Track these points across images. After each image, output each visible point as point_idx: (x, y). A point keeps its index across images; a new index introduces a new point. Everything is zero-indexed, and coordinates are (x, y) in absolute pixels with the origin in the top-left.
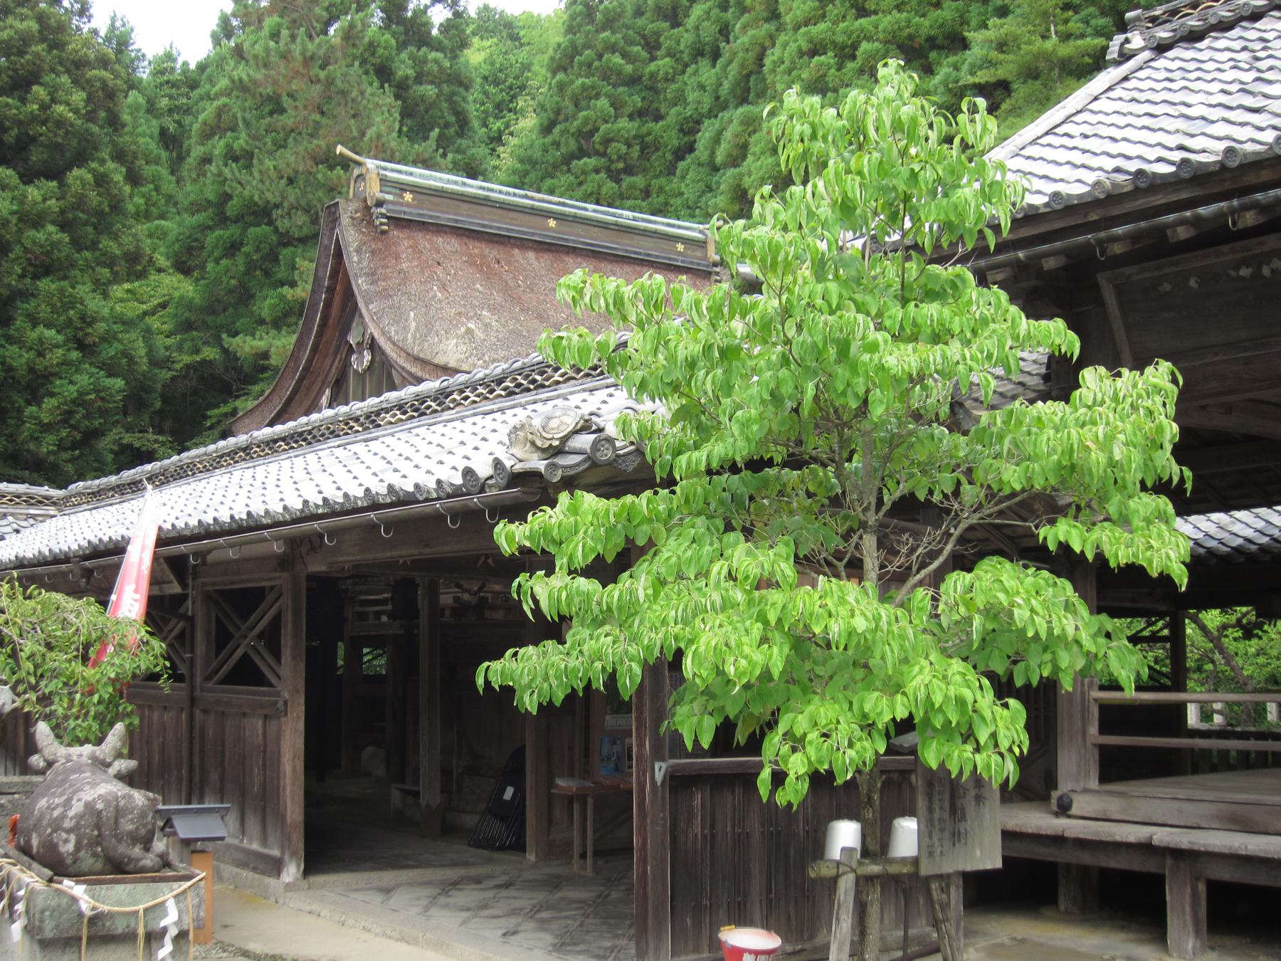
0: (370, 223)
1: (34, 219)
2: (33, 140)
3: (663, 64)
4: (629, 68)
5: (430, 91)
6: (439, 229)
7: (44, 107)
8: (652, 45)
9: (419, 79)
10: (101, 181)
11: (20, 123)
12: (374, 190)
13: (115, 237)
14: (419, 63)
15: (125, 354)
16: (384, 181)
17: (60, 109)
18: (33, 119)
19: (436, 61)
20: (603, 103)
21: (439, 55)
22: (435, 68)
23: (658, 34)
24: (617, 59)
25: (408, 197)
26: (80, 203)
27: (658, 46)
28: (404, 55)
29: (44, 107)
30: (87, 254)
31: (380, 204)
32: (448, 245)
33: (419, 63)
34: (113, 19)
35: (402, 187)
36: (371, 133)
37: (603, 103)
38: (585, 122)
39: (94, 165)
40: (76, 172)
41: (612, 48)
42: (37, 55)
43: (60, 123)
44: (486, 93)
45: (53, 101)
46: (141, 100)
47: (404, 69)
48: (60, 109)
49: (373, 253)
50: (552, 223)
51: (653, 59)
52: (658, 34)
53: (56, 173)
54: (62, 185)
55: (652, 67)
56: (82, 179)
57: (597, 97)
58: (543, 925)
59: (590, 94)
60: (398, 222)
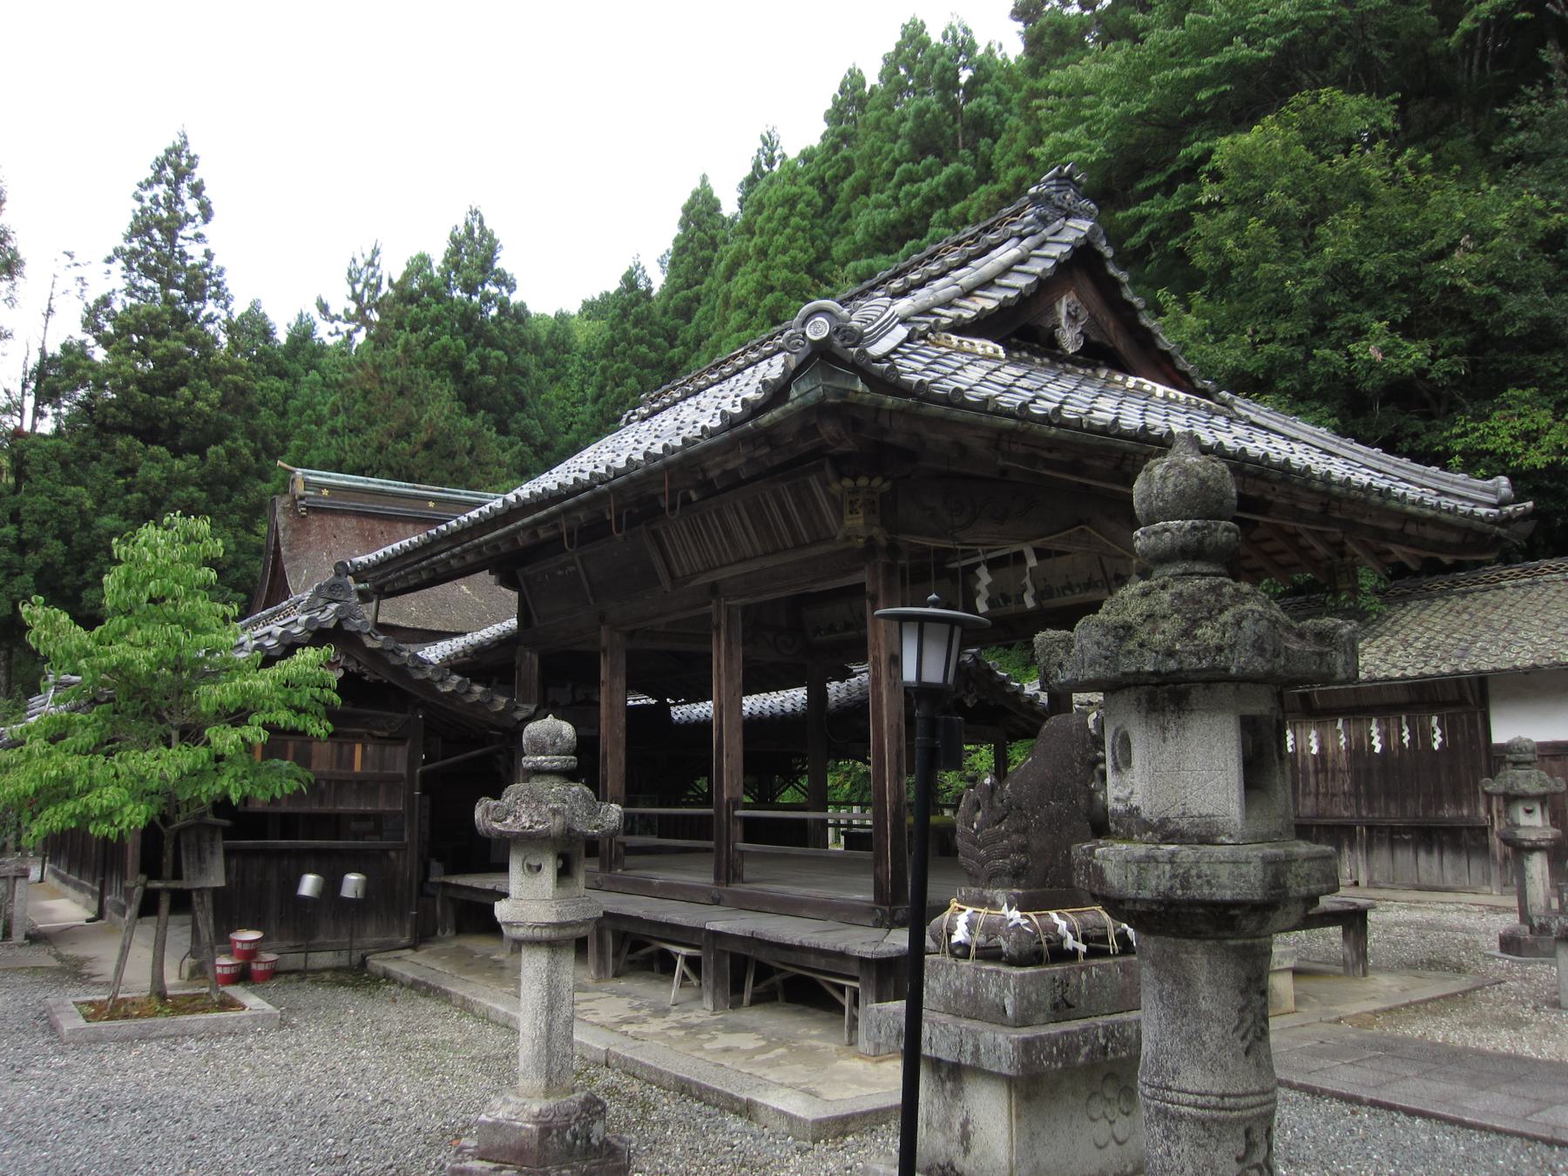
0: (296, 511)
1: (185, 481)
2: (182, 426)
3: (676, 352)
4: (653, 355)
5: (490, 380)
6: (345, 513)
7: (189, 403)
8: (671, 339)
9: (483, 371)
10: (232, 454)
11: (170, 415)
12: (300, 489)
13: (245, 493)
14: (483, 360)
15: (250, 575)
16: (307, 483)
17: (199, 404)
18: (181, 412)
19: (497, 358)
20: (632, 381)
21: (500, 353)
22: (495, 363)
23: (676, 329)
24: (644, 349)
25: (325, 492)
26: (215, 470)
27: (676, 339)
28: (473, 355)
29: (189, 403)
30: (223, 506)
31: (302, 498)
32: (349, 523)
33: (483, 360)
34: (301, 316)
35: (321, 486)
36: (426, 417)
37: (632, 381)
38: (619, 396)
39: (228, 442)
40: (213, 448)
41: (640, 341)
42: (184, 366)
43: (200, 414)
44: (583, 366)
45: (196, 398)
46: (318, 377)
47: (471, 364)
48: (199, 404)
49: (294, 530)
50: (431, 504)
51: (672, 346)
52: (676, 329)
53: (200, 450)
54: (203, 457)
55: (670, 354)
56: (216, 453)
57: (629, 376)
58: (79, 887)
59: (625, 374)
60: (314, 510)
